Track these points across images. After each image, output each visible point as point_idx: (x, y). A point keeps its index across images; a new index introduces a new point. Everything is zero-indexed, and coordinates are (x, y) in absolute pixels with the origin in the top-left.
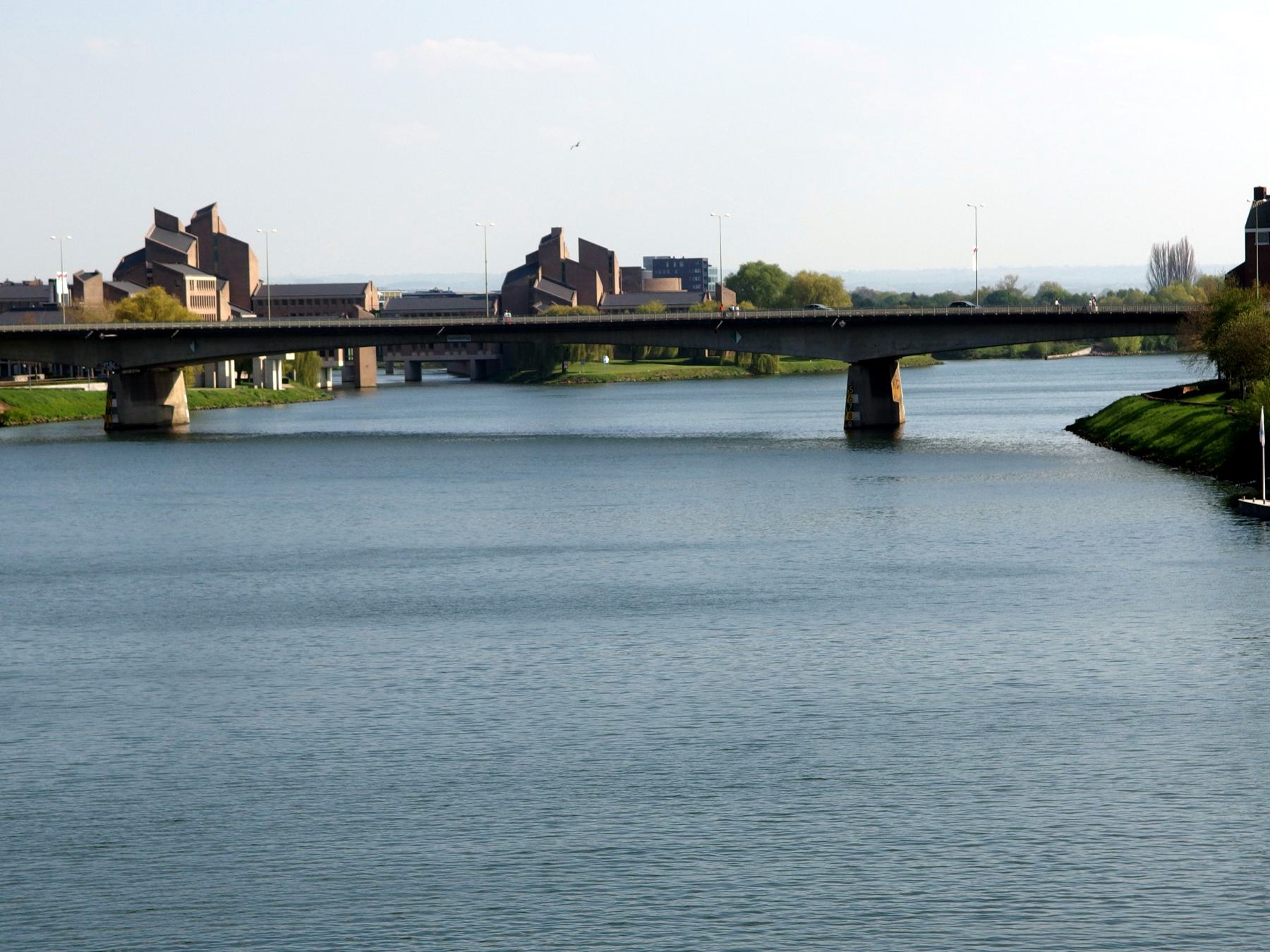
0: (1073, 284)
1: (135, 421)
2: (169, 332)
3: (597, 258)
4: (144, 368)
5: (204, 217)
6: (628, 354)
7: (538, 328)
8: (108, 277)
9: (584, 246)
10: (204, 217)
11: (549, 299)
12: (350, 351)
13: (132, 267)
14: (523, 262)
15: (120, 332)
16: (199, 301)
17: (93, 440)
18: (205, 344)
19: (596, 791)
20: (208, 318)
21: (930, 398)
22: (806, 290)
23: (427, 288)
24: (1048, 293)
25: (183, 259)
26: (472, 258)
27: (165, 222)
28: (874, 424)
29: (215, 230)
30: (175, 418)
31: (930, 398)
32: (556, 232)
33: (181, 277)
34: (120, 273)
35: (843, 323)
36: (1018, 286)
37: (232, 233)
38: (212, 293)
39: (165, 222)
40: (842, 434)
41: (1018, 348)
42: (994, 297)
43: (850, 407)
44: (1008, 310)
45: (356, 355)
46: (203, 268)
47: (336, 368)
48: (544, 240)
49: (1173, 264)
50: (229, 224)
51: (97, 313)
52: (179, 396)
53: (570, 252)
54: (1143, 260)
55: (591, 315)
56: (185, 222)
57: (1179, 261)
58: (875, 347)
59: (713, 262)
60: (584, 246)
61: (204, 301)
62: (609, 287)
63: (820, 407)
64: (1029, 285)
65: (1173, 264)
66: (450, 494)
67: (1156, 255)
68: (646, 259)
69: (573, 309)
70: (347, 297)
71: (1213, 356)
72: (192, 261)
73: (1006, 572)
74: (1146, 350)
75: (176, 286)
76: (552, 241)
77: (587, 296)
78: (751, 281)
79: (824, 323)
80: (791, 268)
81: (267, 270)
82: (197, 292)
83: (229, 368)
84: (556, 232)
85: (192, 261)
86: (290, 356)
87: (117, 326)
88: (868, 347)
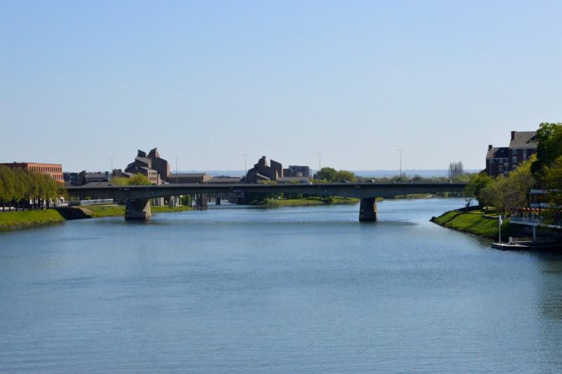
0: (424, 176)
1: (135, 217)
2: (145, 188)
3: (276, 166)
4: (137, 200)
5: (153, 152)
6: (287, 197)
7: (261, 188)
8: (123, 171)
9: (272, 162)
10: (153, 152)
11: (262, 179)
12: (199, 195)
13: (131, 168)
14: (253, 167)
15: (130, 188)
16: (153, 179)
17: (115, 223)
18: (155, 191)
19: (333, 349)
20: (154, 184)
21: (383, 208)
22: (344, 176)
23: (221, 175)
24: (417, 179)
25: (147, 165)
26: (238, 165)
27: (141, 154)
28: (368, 217)
29: (156, 156)
30: (147, 215)
31: (383, 208)
32: (264, 158)
33: (146, 171)
34: (126, 170)
35: (166, 202)
36: (407, 175)
37: (162, 157)
38: (156, 176)
39: (141, 154)
40: (358, 220)
41: (408, 196)
42: (399, 179)
43: (361, 213)
44: (419, 183)
45: (201, 196)
46: (153, 168)
47: (194, 200)
48: (261, 160)
49: (456, 170)
50: (162, 155)
51: (123, 183)
52: (148, 210)
53: (269, 165)
54: (447, 168)
55: (274, 183)
56: (147, 154)
57: (458, 169)
58: (369, 194)
59: (311, 168)
60: (272, 162)
61: (153, 179)
62: (280, 176)
63: (353, 211)
64: (410, 176)
65: (456, 170)
66: (226, 238)
67: (451, 166)
68: (290, 166)
69: (267, 182)
70: (198, 178)
71: (477, 199)
72: (150, 166)
73: (75, 239)
74: (450, 196)
75: (145, 173)
76: (262, 160)
77: (273, 178)
78: (326, 173)
79: (352, 186)
80: (338, 169)
81: (174, 168)
82: (151, 176)
83: (162, 199)
84: (264, 158)
85: (150, 166)
86: (182, 196)
87: (129, 186)
88: (368, 194)
